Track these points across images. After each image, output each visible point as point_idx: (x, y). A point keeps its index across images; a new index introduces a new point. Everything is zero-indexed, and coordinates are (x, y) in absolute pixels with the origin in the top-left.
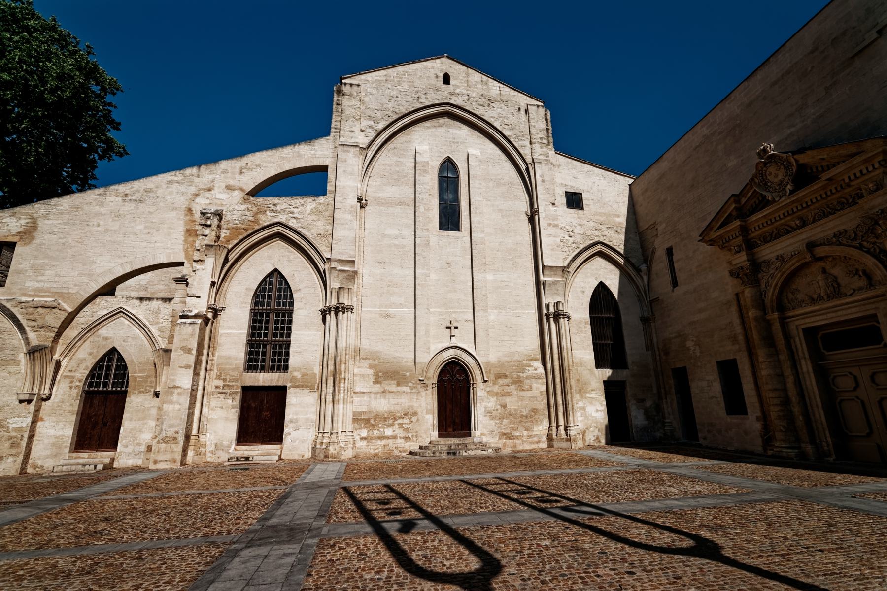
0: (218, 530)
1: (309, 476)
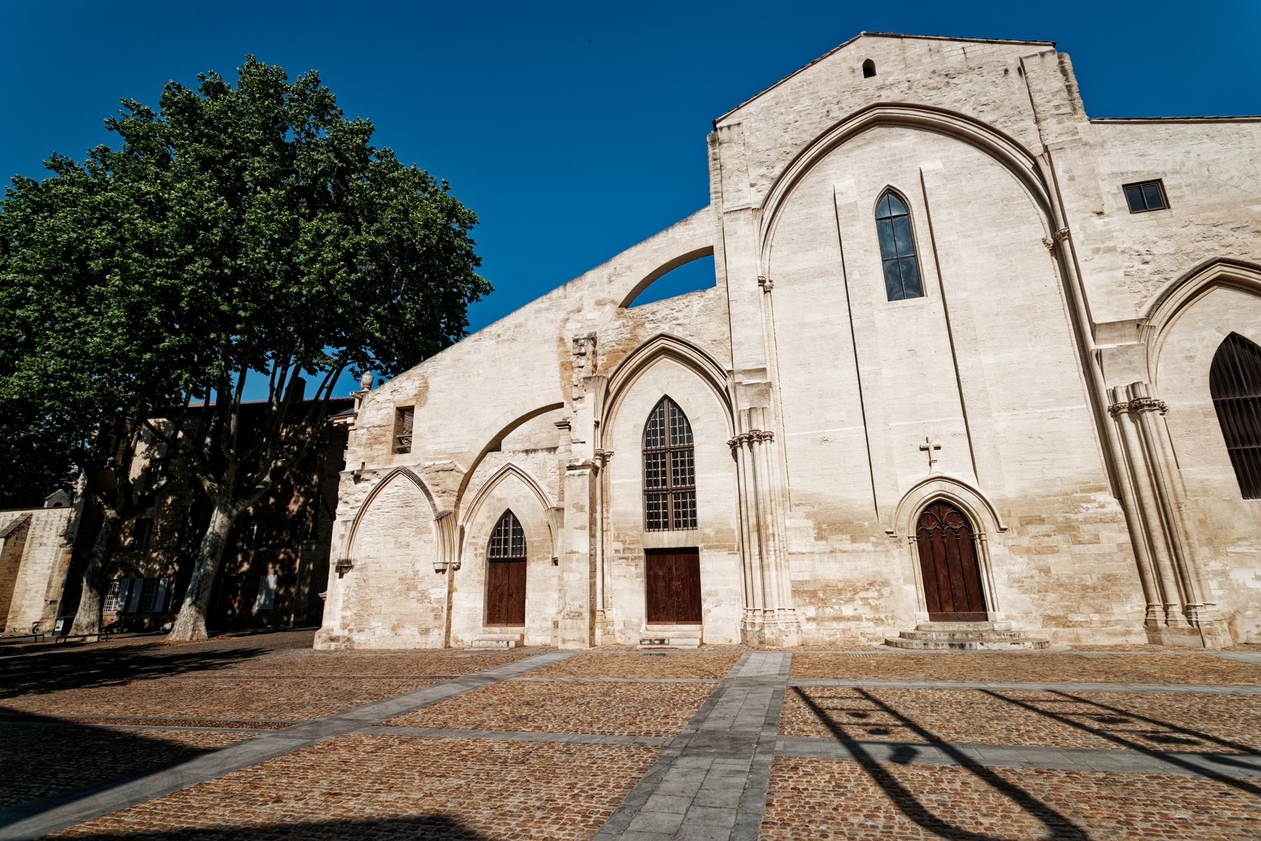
0: (645, 729)
1: (744, 669)
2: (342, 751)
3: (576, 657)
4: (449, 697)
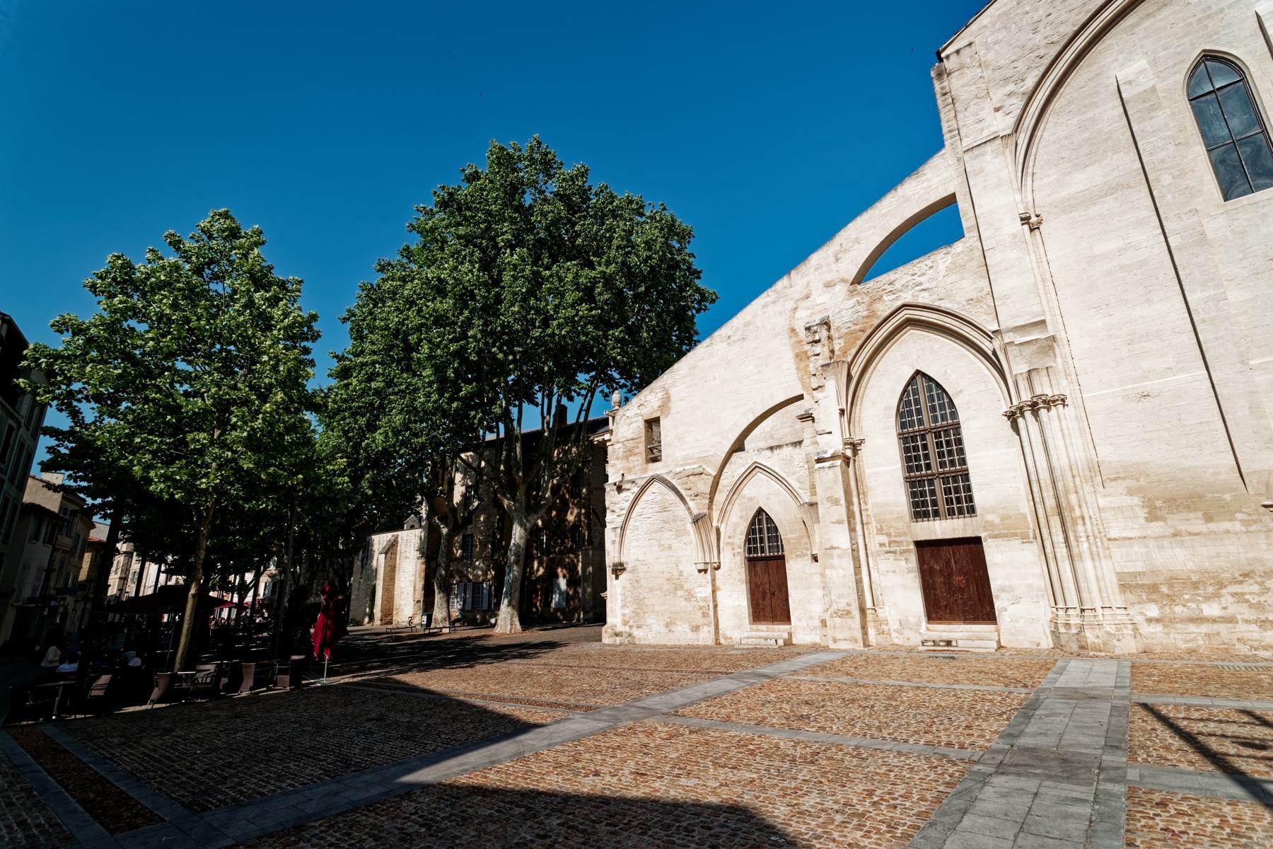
0: (944, 739)
2: (641, 735)
3: (849, 657)
4: (728, 692)
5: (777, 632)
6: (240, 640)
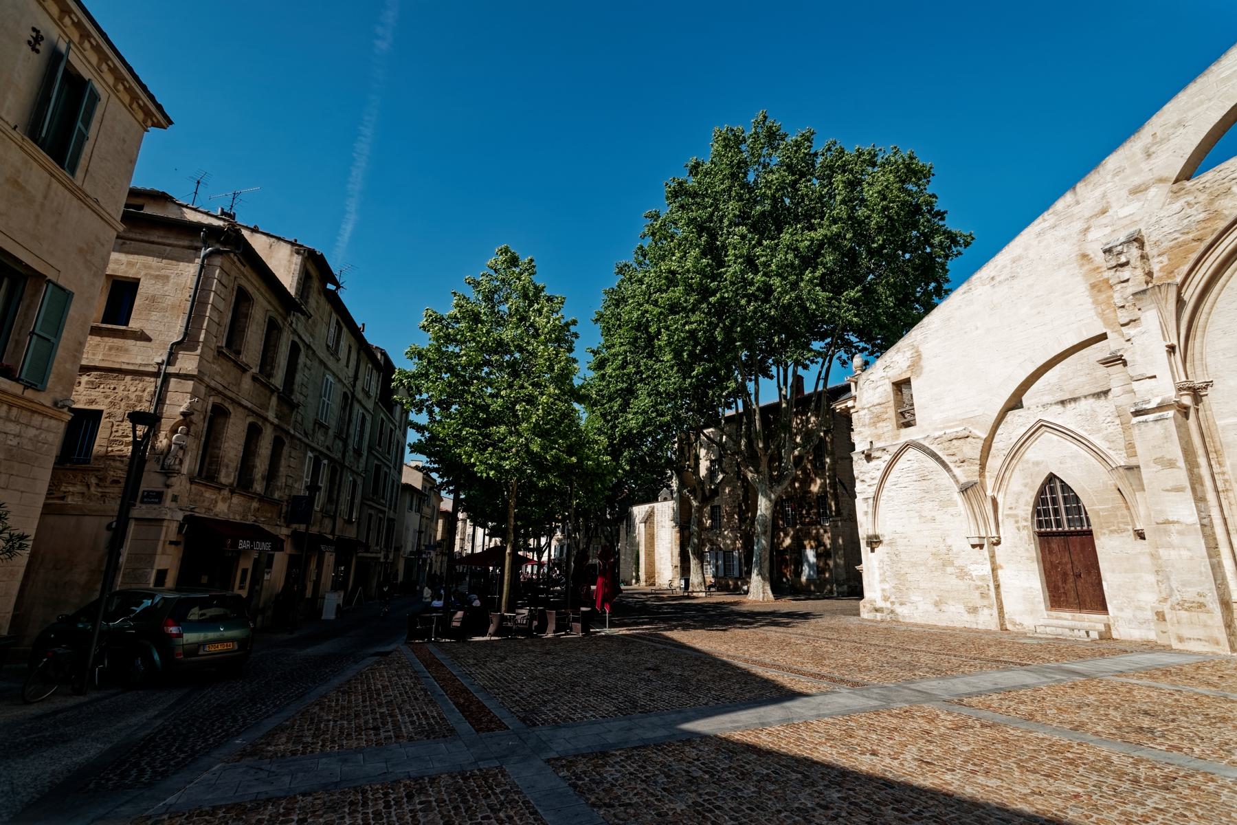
2: (919, 720)
4: (1026, 686)
5: (1090, 622)
6: (542, 592)
